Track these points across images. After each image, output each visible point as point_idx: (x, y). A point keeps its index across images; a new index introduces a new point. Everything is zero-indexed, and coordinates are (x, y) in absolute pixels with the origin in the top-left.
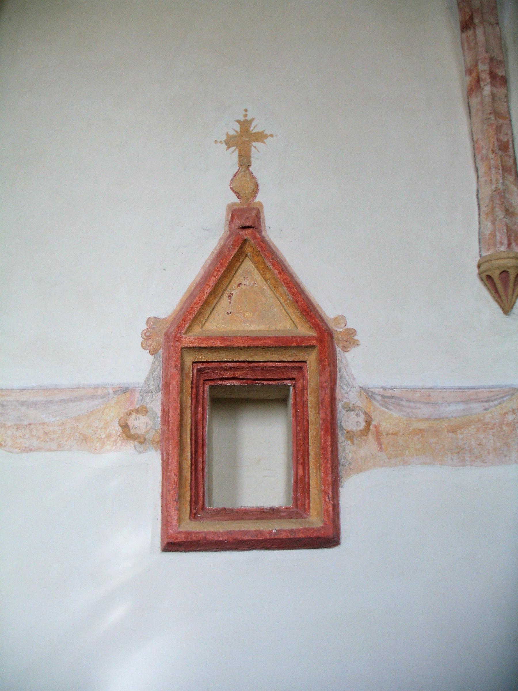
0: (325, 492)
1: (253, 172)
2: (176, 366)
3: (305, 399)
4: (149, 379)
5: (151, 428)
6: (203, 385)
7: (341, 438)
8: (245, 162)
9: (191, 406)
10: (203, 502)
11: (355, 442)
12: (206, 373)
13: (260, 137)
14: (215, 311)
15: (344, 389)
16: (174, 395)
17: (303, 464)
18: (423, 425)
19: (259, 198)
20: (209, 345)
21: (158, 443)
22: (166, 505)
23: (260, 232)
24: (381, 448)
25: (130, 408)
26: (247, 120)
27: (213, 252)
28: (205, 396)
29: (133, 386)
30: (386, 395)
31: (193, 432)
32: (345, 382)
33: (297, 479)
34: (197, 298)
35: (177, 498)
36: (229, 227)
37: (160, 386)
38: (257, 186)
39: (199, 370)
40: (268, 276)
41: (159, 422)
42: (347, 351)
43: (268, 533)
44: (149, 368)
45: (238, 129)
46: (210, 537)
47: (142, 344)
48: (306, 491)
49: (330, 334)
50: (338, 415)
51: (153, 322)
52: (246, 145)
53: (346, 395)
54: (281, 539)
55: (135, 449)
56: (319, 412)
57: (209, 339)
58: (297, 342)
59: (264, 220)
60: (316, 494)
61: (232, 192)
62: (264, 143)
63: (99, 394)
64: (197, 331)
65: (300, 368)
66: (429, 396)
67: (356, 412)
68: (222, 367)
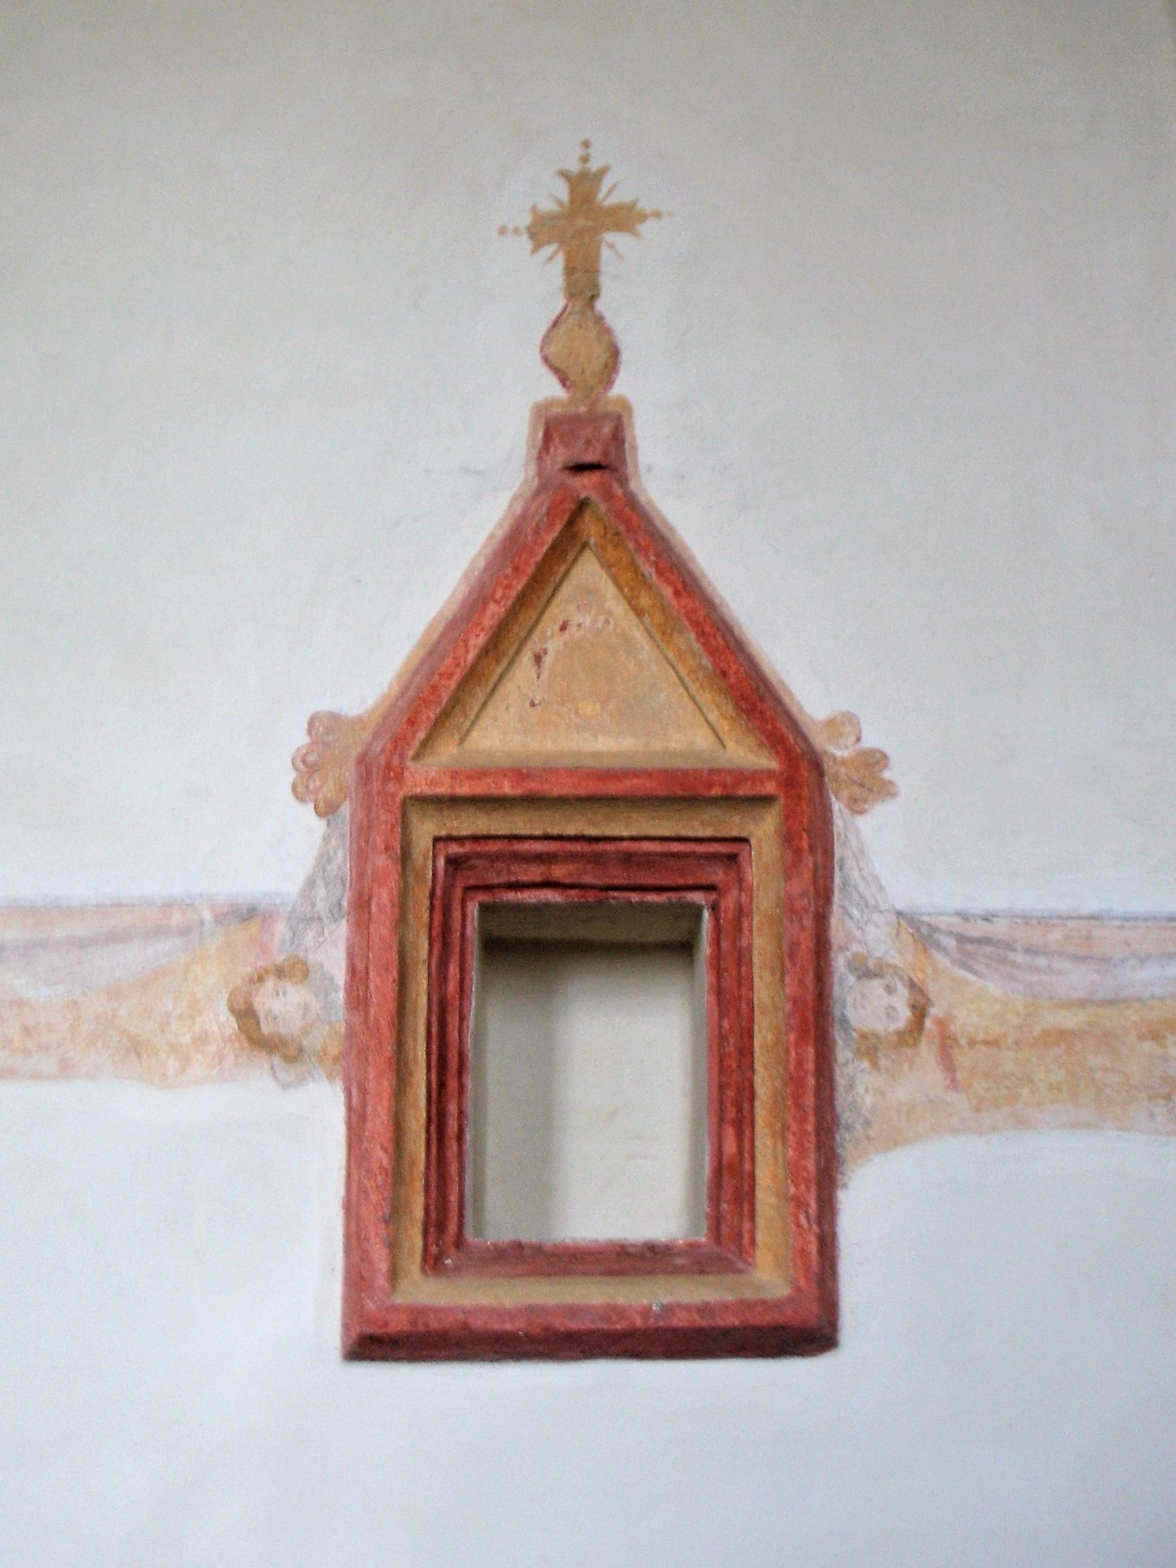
0: (799, 1203)
2: (387, 848)
3: (744, 944)
4: (315, 881)
5: (318, 1018)
6: (463, 902)
7: (843, 1053)
8: (583, 286)
11: (883, 1062)
13: (626, 218)
14: (497, 697)
15: (851, 917)
16: (382, 928)
18: (1071, 1020)
19: (621, 387)
23: (623, 481)
24: (953, 1080)
25: (260, 964)
27: (492, 536)
28: (469, 932)
31: (434, 1030)
32: (856, 896)
37: (345, 904)
38: (615, 353)
39: (454, 863)
40: (644, 601)
48: (745, 1197)
49: (817, 765)
51: (324, 727)
53: (858, 934)
55: (274, 1074)
56: (782, 980)
57: (480, 774)
58: (724, 786)
59: (634, 448)
64: (447, 752)
66: (1089, 937)
67: (888, 980)
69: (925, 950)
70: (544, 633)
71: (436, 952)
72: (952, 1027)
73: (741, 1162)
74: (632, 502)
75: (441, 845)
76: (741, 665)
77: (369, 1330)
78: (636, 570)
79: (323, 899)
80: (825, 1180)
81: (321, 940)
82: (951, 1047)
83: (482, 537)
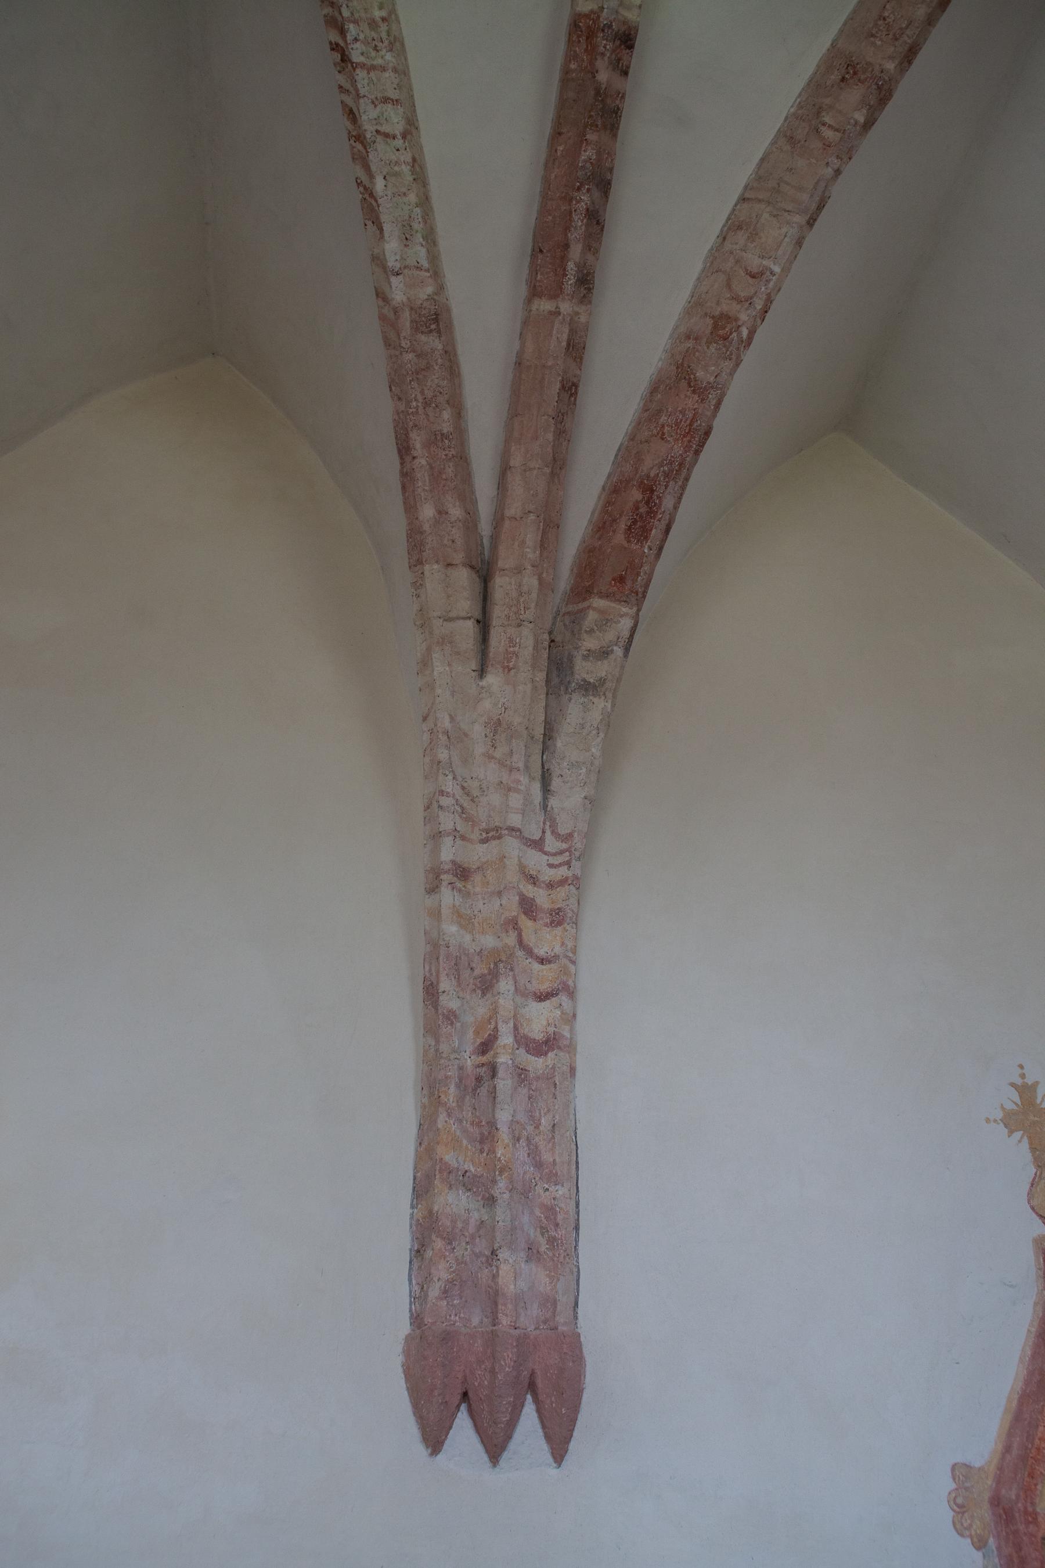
61: (1034, 1215)
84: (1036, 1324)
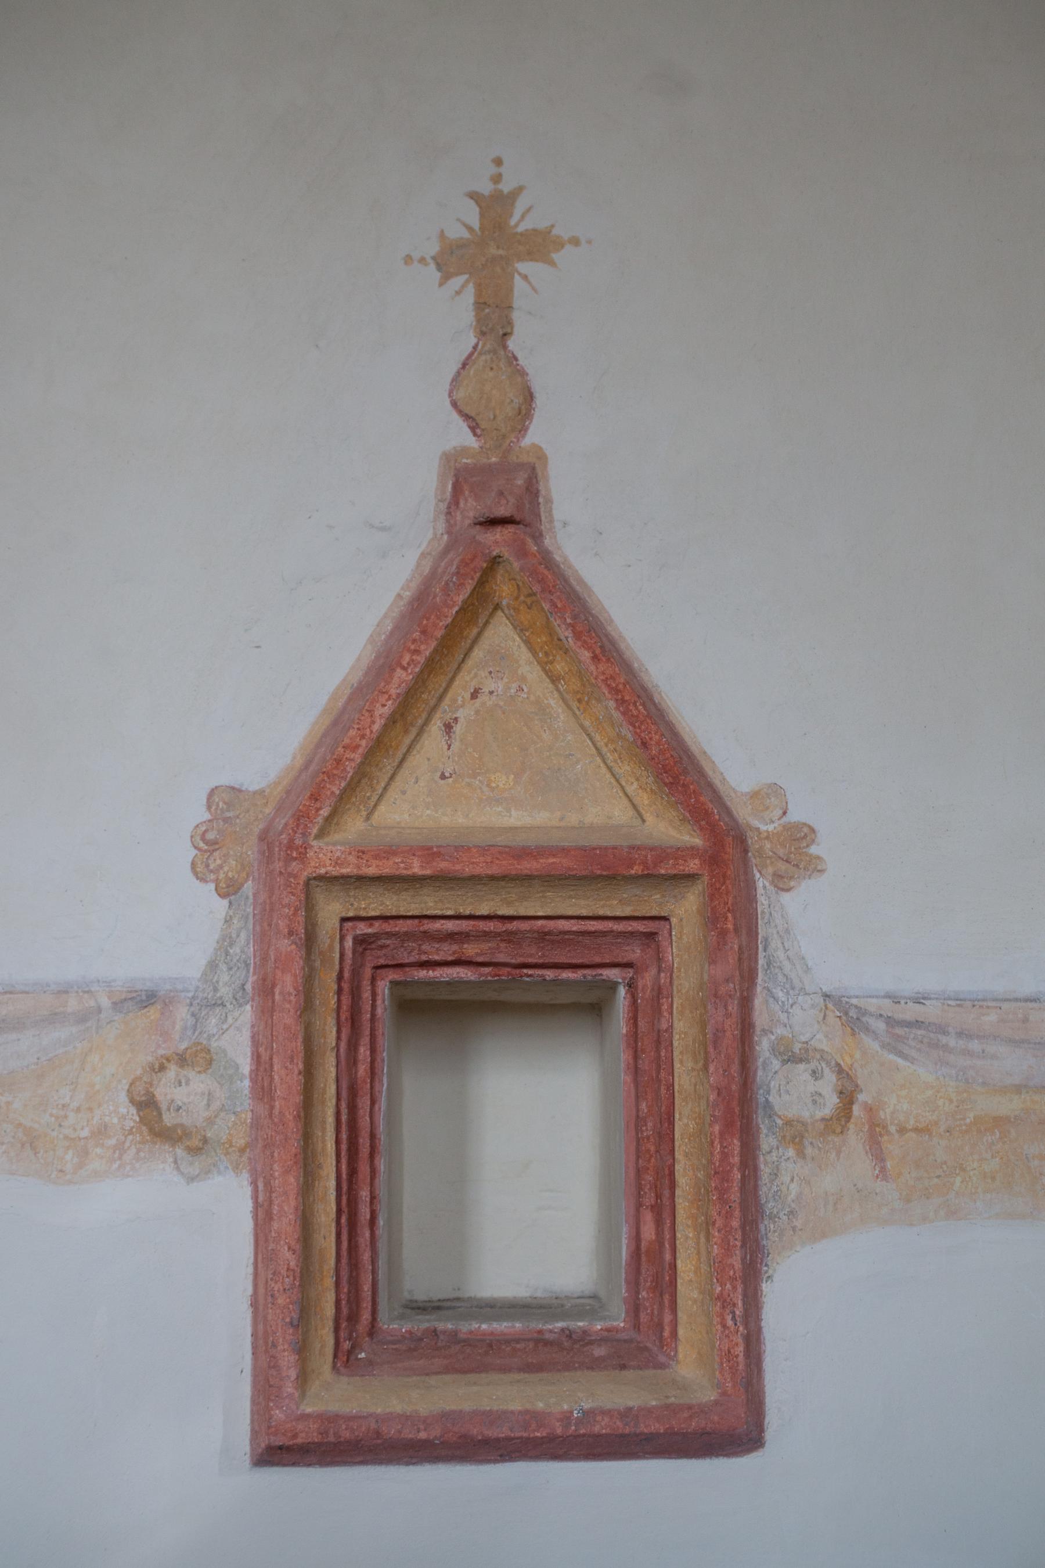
0: (724, 1301)
1: (519, 355)
2: (291, 933)
3: (664, 1026)
4: (217, 966)
5: (223, 1108)
6: (373, 980)
7: (767, 1141)
8: (494, 322)
9: (337, 1045)
10: (374, 1312)
11: (809, 1151)
12: (382, 947)
13: (540, 245)
14: (404, 772)
15: (776, 1000)
16: (287, 1017)
17: (657, 1210)
18: (1008, 1106)
19: (534, 436)
20: (386, 871)
21: (242, 1151)
22: (266, 1333)
23: (538, 537)
24: (883, 1169)
25: (161, 1052)
26: (501, 191)
27: (399, 596)
28: (379, 1011)
29: (168, 987)
30: (899, 1016)
31: (344, 1118)
32: (780, 977)
33: (638, 1248)
34: (352, 733)
35: (295, 1316)
36: (447, 521)
37: (249, 987)
38: (529, 397)
39: (362, 941)
40: (560, 666)
41: (247, 1092)
42: (788, 890)
43: (561, 1420)
44: (217, 937)
45: (475, 222)
46: (391, 1431)
47: (193, 865)
48: (665, 1285)
49: (741, 841)
50: (760, 1073)
51: (225, 801)
52: (498, 270)
53: (783, 1017)
54: (599, 1436)
55: (178, 1169)
56: (706, 1067)
57: (388, 852)
58: (644, 863)
59: (549, 501)
60: (695, 1301)
61: (455, 416)
62: (552, 263)
63: (69, 1010)
64: (353, 827)
65: (651, 935)
66: (1025, 1020)
67: (814, 1064)
68: (425, 932)
69: (853, 1034)
70: (455, 700)
71: (344, 1036)
72: (882, 1114)
73: (661, 1252)
74: (546, 559)
75: (349, 925)
76: (662, 735)
77: (278, 1441)
78: (552, 633)
79: (226, 984)
80: (752, 1275)
81: (225, 1027)
82: (881, 1135)
83: (388, 599)
84: (414, 585)
